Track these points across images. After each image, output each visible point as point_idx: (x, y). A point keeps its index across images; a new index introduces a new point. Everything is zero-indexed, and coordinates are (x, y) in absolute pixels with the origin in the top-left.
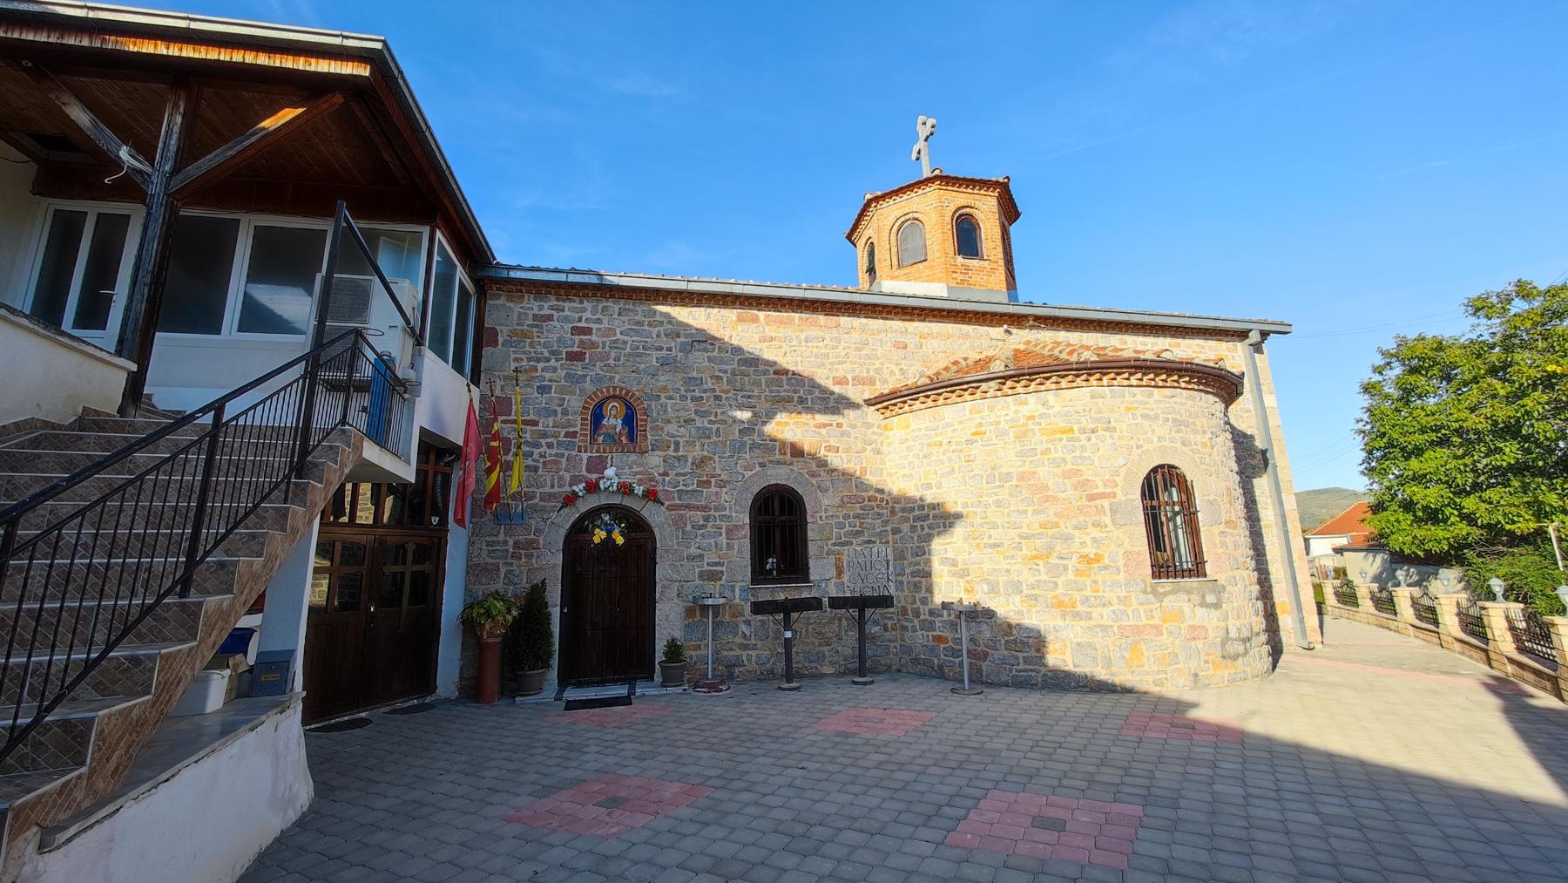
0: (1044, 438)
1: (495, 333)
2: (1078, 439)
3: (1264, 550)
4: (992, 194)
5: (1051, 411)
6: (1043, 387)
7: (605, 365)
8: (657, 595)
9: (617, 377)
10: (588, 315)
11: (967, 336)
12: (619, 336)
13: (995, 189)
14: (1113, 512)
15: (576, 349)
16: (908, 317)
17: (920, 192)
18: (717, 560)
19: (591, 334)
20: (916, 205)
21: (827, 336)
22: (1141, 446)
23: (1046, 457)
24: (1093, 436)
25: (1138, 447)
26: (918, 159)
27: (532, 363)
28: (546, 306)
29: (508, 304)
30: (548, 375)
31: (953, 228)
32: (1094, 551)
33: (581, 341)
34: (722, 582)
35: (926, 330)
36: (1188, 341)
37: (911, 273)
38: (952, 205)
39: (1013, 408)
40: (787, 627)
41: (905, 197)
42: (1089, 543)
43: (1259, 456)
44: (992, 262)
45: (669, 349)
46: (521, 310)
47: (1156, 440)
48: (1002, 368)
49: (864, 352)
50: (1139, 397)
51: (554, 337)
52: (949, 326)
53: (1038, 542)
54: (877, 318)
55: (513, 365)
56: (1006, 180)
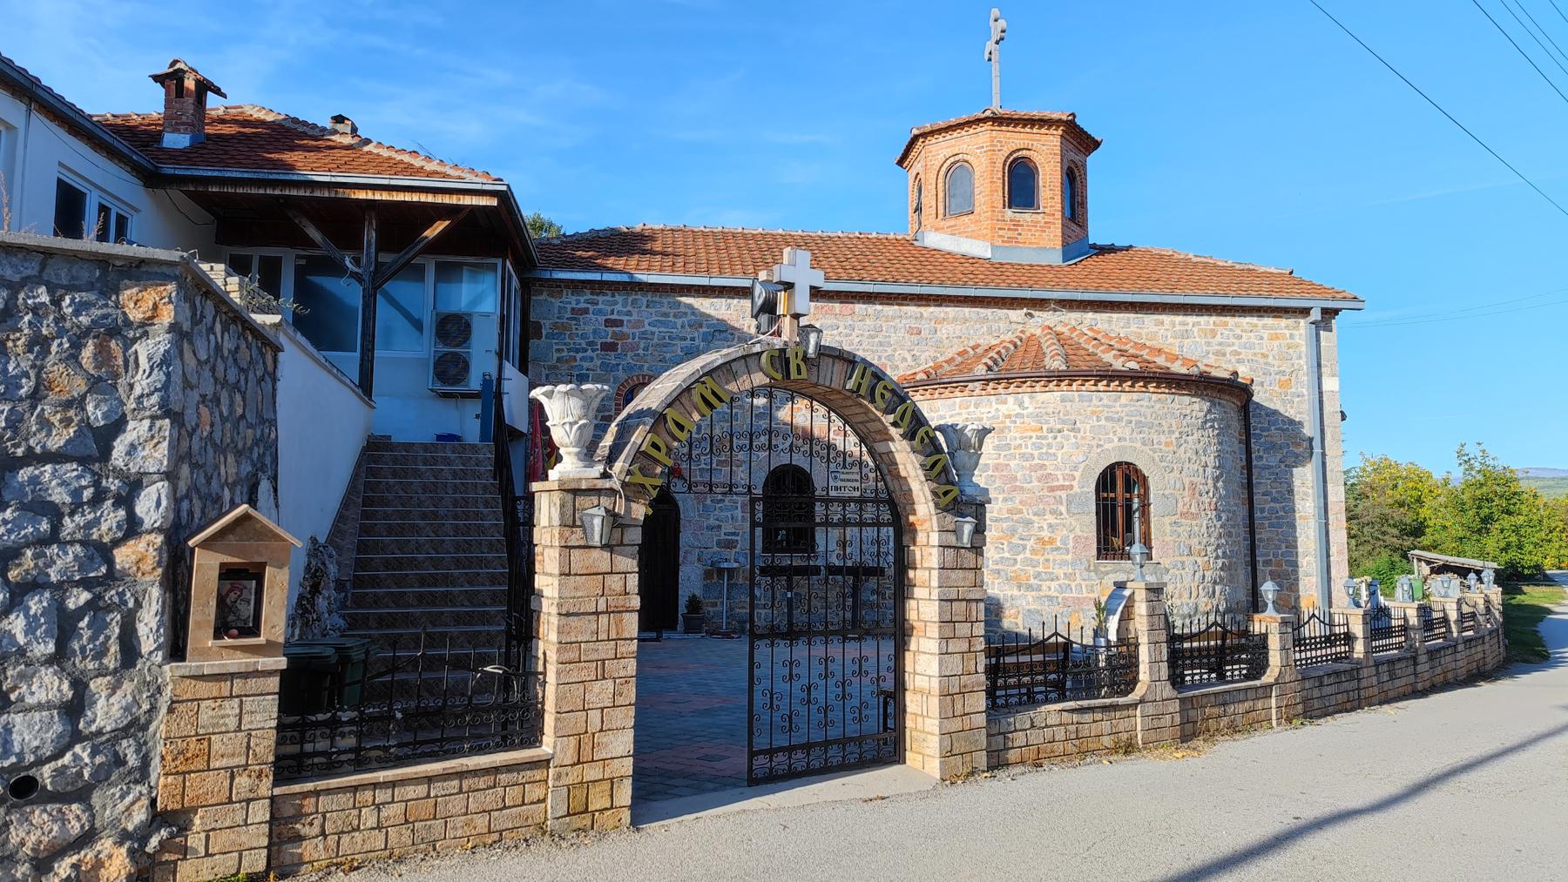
0: (1018, 435)
1: (538, 327)
2: (1045, 438)
3: (1296, 542)
4: (1055, 132)
5: (1025, 412)
6: (1020, 390)
7: (635, 355)
8: (681, 559)
9: (646, 365)
10: (618, 307)
11: (986, 319)
12: (647, 327)
13: (1059, 127)
14: (1069, 503)
15: (609, 340)
16: (924, 303)
17: (971, 131)
18: (733, 530)
19: (622, 326)
20: (965, 146)
21: (841, 324)
22: (1102, 446)
23: (1018, 451)
24: (1059, 435)
25: (1098, 446)
26: (990, 60)
27: (571, 354)
28: (582, 299)
29: (550, 299)
30: (585, 365)
31: (1004, 176)
32: (1049, 535)
33: (614, 332)
34: (737, 550)
35: (942, 315)
36: (1237, 319)
37: (955, 226)
38: (1005, 148)
39: (995, 406)
40: (790, 588)
41: (955, 134)
42: (1045, 527)
43: (1305, 444)
44: (1049, 215)
45: (693, 339)
46: (561, 305)
47: (1116, 440)
48: (984, 372)
49: (876, 340)
50: (1105, 401)
51: (589, 329)
52: (967, 310)
53: (1005, 525)
54: (892, 304)
55: (556, 355)
56: (1070, 118)
